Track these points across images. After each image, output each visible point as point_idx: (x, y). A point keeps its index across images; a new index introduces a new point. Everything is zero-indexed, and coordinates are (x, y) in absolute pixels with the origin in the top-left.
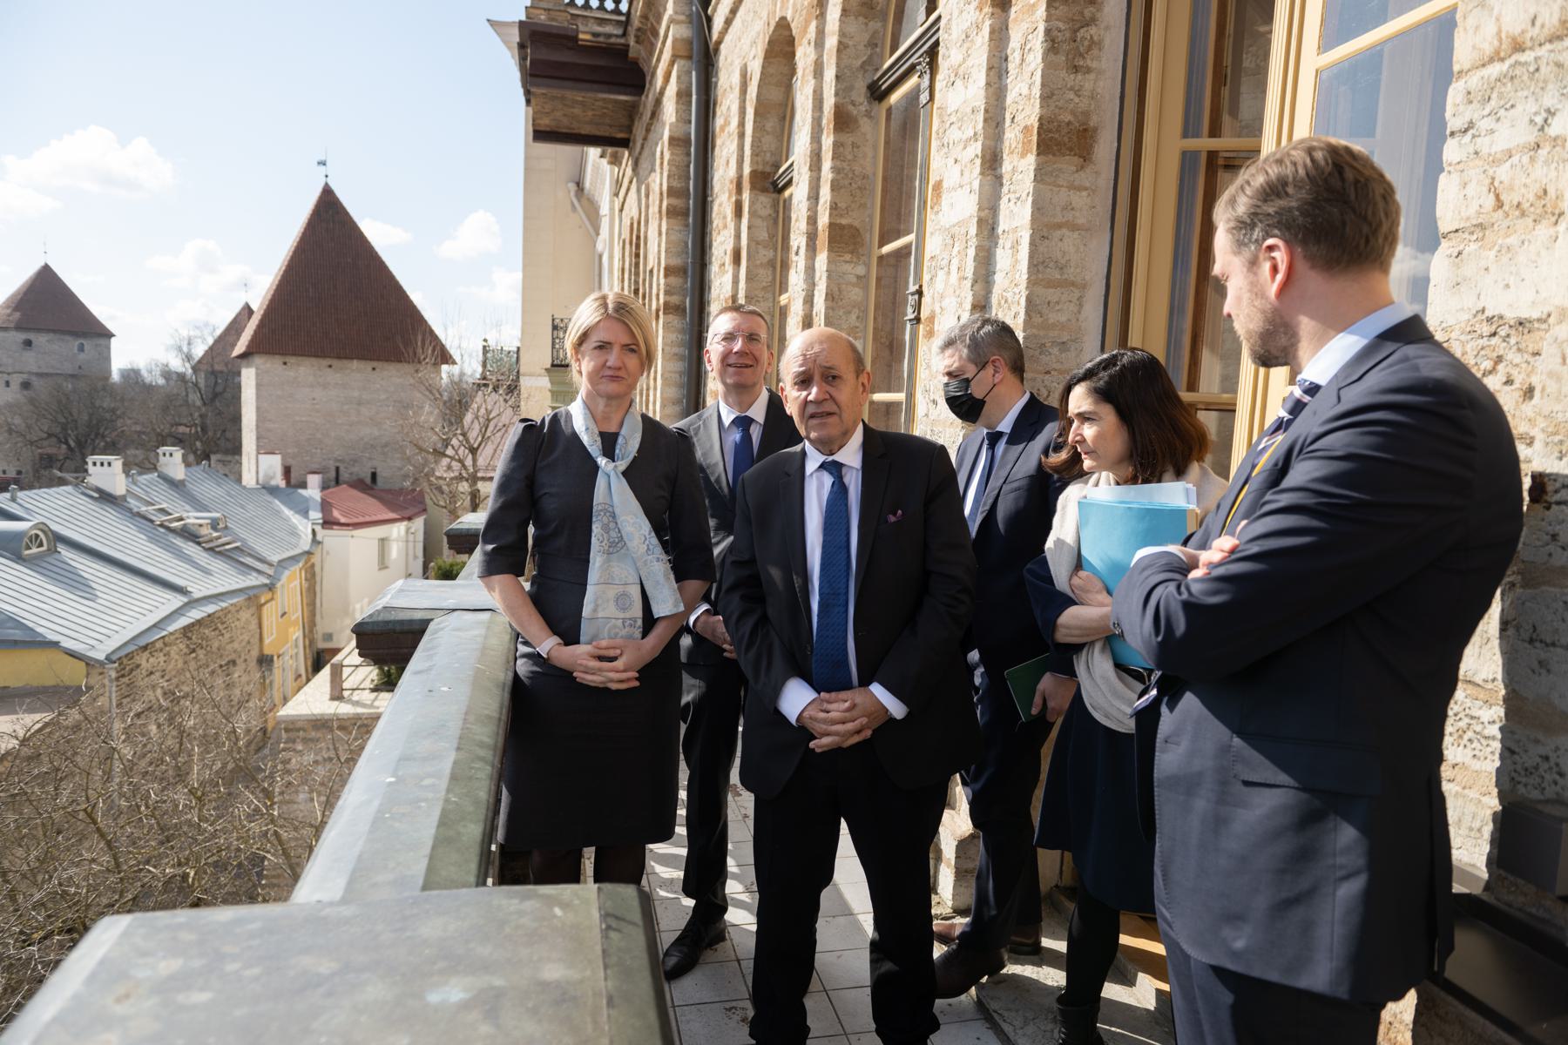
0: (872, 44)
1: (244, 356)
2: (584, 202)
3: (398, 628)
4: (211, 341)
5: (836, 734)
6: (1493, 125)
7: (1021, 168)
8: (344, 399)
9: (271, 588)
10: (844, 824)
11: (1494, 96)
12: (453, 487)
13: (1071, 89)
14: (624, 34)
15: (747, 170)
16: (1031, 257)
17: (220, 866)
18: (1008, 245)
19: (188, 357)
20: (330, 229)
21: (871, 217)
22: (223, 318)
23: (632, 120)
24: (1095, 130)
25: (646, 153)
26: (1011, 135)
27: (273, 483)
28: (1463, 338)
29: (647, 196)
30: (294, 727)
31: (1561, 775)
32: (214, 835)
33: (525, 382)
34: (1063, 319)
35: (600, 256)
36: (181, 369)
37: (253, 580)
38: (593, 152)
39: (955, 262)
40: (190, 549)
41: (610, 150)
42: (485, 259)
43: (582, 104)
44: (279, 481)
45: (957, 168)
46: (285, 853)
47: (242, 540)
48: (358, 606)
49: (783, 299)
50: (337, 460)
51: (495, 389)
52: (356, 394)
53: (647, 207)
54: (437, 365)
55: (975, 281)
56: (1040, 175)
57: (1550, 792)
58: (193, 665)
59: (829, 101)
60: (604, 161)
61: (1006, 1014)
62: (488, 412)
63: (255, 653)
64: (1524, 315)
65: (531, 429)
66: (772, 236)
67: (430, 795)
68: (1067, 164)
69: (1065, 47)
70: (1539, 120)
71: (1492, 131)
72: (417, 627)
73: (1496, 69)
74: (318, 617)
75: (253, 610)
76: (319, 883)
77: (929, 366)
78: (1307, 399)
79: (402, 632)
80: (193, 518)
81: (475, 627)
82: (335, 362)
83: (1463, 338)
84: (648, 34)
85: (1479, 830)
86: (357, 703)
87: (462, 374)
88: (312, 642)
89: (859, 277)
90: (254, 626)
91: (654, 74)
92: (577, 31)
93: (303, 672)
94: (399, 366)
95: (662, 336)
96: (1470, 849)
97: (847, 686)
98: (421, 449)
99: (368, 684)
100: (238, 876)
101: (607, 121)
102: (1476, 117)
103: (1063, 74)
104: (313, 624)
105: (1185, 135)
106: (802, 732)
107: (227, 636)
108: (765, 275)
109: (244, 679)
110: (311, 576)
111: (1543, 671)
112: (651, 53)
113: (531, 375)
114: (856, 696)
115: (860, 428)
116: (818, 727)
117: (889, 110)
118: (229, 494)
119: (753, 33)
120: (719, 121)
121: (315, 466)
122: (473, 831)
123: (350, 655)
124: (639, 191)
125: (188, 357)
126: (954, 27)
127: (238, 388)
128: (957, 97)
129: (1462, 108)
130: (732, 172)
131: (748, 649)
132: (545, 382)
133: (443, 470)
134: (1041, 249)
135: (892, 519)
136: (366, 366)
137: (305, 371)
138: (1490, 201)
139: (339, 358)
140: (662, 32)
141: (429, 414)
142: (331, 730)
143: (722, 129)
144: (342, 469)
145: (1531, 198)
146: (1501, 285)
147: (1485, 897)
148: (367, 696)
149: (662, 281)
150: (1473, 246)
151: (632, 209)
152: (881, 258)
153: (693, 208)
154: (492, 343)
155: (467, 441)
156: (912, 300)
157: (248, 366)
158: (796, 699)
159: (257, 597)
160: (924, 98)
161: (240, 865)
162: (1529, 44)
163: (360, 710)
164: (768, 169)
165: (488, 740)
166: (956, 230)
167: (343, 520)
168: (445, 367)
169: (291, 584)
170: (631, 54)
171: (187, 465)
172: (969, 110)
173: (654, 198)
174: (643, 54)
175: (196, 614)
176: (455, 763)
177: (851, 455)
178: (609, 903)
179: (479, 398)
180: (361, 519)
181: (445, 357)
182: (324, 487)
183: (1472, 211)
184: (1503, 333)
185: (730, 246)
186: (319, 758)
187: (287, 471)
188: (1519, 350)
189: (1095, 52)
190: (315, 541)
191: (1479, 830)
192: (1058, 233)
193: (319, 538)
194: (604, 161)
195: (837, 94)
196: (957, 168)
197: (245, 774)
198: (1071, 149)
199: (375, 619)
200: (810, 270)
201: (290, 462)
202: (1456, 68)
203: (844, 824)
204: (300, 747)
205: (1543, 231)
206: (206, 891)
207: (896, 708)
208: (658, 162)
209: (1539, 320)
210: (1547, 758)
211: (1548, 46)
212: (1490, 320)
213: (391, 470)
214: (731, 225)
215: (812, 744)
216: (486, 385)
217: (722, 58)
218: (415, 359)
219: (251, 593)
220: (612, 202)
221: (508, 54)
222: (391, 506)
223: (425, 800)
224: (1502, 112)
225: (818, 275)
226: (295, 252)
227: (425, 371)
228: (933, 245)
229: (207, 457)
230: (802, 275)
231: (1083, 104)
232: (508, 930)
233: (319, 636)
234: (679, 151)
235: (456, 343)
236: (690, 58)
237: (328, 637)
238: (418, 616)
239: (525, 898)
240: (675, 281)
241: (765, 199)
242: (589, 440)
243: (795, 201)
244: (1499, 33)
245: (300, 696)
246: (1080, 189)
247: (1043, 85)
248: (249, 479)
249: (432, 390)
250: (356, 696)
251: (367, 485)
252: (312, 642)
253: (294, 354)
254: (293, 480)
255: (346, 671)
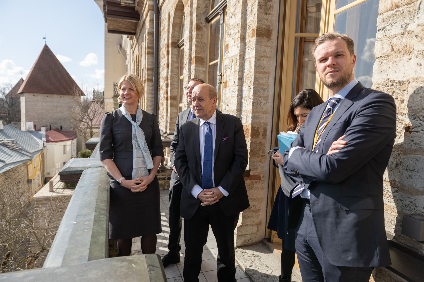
0: (206, 7)
1: (21, 93)
2: (122, 50)
3: (73, 173)
4: (11, 89)
5: (209, 201)
6: (391, 28)
7: (251, 41)
8: (52, 105)
9: (31, 160)
10: (210, 226)
11: (391, 20)
12: (85, 131)
13: (265, 19)
14: (134, 3)
15: (170, 42)
16: (255, 65)
17: (17, 242)
18: (248, 62)
19: (4, 94)
20: (47, 58)
21: (207, 55)
22: (15, 82)
23: (136, 28)
24: (272, 30)
25: (141, 37)
26: (249, 32)
27: (31, 130)
28: (383, 86)
29: (141, 49)
30: (38, 200)
31: (416, 207)
32: (14, 234)
33: (106, 101)
34: (264, 82)
35: (127, 66)
36: (2, 97)
37: (25, 158)
38: (125, 36)
39: (233, 67)
40: (5, 149)
41: (130, 36)
42: (91, 67)
43: (122, 23)
44: (33, 129)
45: (233, 40)
46: (37, 237)
47: (22, 146)
48: (57, 165)
49: (181, 77)
50: (50, 123)
51: (97, 103)
52: (56, 104)
53: (141, 52)
54: (80, 96)
55: (239, 72)
56: (257, 43)
57: (413, 212)
58: (7, 183)
59: (194, 22)
60: (128, 39)
61: (253, 276)
62: (95, 109)
63: (26, 179)
64: (401, 80)
65: (109, 115)
66: (178, 60)
67: (88, 227)
68: (264, 40)
69: (263, 7)
70: (404, 26)
71: (390, 30)
72: (78, 173)
73: (391, 12)
74: (45, 169)
75: (25, 166)
76: (53, 261)
77: (225, 95)
78: (336, 103)
79: (74, 174)
80: (6, 140)
81: (96, 171)
82: (49, 95)
83: (383, 86)
84: (141, 4)
85: (391, 222)
86: (58, 193)
87: (87, 98)
88: (43, 175)
89: (203, 71)
90: (26, 171)
91: (143, 15)
92: (120, 2)
93: (41, 184)
94: (69, 96)
95: (146, 88)
96: (390, 228)
97: (212, 187)
98: (76, 120)
99: (61, 187)
100: (22, 245)
101: (129, 27)
102: (385, 25)
103: (263, 15)
104: (43, 170)
105: (296, 32)
106: (199, 201)
107: (17, 174)
108: (176, 71)
109: (23, 187)
110: (43, 157)
111: (410, 178)
112: (142, 9)
113: (108, 99)
114: (214, 190)
115: (215, 112)
116: (203, 199)
117: (211, 25)
118: (17, 133)
119: (171, 4)
120: (162, 28)
121: (43, 125)
122: (103, 239)
123: (56, 178)
124: (139, 47)
125: (4, 94)
126: (231, 2)
127: (20, 103)
128: (232, 20)
129: (381, 23)
130: (166, 42)
131: (182, 177)
132: (112, 101)
133: (82, 125)
134: (258, 63)
135: (225, 139)
136: (59, 96)
137: (40, 98)
138: (390, 49)
139: (50, 94)
140: (145, 3)
141: (78, 110)
142: (50, 201)
143: (163, 30)
144: (52, 126)
145: (402, 48)
146: (394, 72)
147: (394, 241)
148: (61, 191)
149: (146, 72)
150: (385, 61)
151: (136, 52)
152: (210, 66)
153: (155, 52)
154: (96, 90)
155: (89, 117)
156: (218, 78)
157: (23, 96)
158: (197, 191)
159: (26, 163)
160: (221, 22)
161: (23, 242)
162: (401, 5)
163: (59, 195)
164: (176, 41)
165: (105, 208)
166: (233, 58)
167: (52, 140)
168: (82, 97)
169: (37, 158)
170: (136, 9)
171: (4, 125)
172: (236, 24)
173: (143, 49)
174: (139, 9)
175: (7, 168)
176: (95, 216)
177: (213, 120)
178: (149, 261)
179: (93, 104)
180: (58, 140)
181: (82, 94)
182: (46, 131)
183: (385, 52)
184: (395, 85)
185: (166, 62)
186: (47, 209)
187: (35, 126)
188: (399, 89)
189: (271, 9)
190: (44, 146)
191: (391, 222)
192: (262, 59)
193: (45, 145)
194: (128, 39)
195: (197, 20)
196: (233, 40)
197: (24, 215)
198: (265, 36)
199: (66, 170)
200: (190, 69)
201: (36, 124)
202: (379, 12)
203: (210, 226)
204: (40, 206)
205: (406, 57)
206: (12, 250)
207: (226, 193)
208: (144, 39)
209: (405, 81)
210: (412, 202)
211: (406, 6)
212: (391, 81)
213: (65, 126)
214: (166, 57)
215: (201, 204)
216: (94, 102)
217: (162, 11)
218: (73, 94)
219: (25, 162)
220: (130, 51)
221: (99, 9)
222: (66, 136)
223: (86, 229)
224: (393, 24)
225: (192, 70)
226: (31, 74)
227: (76, 98)
228: (226, 62)
229: (10, 123)
230: (188, 71)
231: (268, 23)
232: (118, 273)
233: (45, 173)
234: (150, 36)
235: (85, 90)
236: (153, 10)
237: (48, 174)
238: (79, 169)
239: (123, 261)
240: (150, 72)
241: (176, 50)
242: (129, 118)
243: (185, 50)
244: (392, 2)
245: (41, 191)
246: (268, 46)
247: (258, 18)
248: (23, 128)
249: (79, 103)
250: (58, 190)
251: (59, 130)
252: (43, 175)
253: (37, 93)
254: (37, 129)
255: (54, 184)
